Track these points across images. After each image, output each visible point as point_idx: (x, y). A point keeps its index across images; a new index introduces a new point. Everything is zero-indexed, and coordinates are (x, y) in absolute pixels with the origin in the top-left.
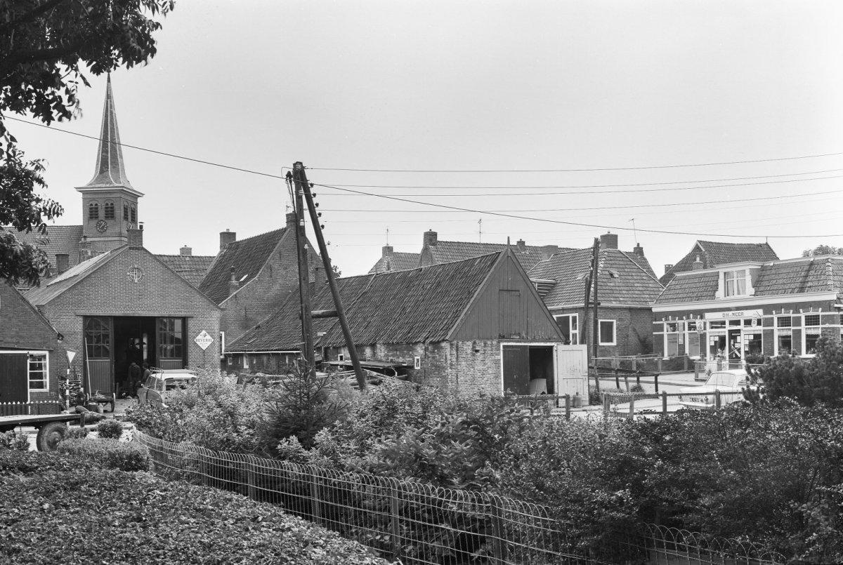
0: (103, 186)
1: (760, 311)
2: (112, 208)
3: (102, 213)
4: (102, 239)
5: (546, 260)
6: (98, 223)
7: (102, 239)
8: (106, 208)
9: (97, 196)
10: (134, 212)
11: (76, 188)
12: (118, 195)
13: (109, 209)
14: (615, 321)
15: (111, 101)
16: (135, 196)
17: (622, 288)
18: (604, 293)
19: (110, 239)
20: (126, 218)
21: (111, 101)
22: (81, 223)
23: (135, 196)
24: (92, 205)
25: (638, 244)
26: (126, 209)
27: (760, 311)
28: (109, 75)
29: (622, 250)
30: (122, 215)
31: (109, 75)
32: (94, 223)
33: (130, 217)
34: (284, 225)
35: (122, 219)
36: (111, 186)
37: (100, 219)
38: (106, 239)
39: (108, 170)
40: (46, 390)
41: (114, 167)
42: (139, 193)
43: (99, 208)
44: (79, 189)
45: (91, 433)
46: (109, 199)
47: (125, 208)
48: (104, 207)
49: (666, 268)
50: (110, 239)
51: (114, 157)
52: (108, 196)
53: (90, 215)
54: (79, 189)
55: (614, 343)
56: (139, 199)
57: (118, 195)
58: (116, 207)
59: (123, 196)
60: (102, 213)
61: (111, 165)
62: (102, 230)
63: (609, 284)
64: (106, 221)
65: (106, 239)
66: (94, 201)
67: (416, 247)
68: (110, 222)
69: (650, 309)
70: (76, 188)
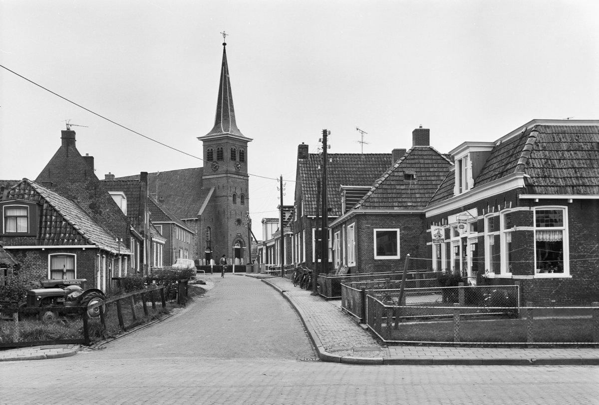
0: (216, 135)
1: (474, 212)
2: (222, 151)
3: (215, 156)
4: (215, 176)
5: (158, 183)
7: (215, 176)
8: (218, 152)
9: (212, 143)
10: (243, 154)
11: (198, 138)
12: (226, 141)
13: (220, 153)
14: (398, 230)
15: (225, 68)
16: (244, 142)
17: (416, 191)
18: (424, 193)
19: (220, 176)
20: (233, 158)
21: (225, 68)
22: (202, 166)
23: (244, 142)
24: (209, 150)
25: (68, 137)
27: (474, 212)
28: (224, 47)
30: (230, 156)
31: (224, 47)
33: (238, 159)
34: (391, 153)
37: (214, 160)
38: (218, 176)
41: (225, 120)
42: (249, 139)
46: (220, 144)
50: (220, 176)
51: (226, 111)
52: (220, 142)
53: (208, 158)
55: (377, 258)
56: (248, 143)
57: (226, 141)
58: (224, 151)
60: (215, 156)
61: (223, 118)
62: (215, 169)
63: (398, 187)
65: (218, 176)
67: (108, 174)
68: (220, 163)
69: (422, 215)
70: (198, 138)
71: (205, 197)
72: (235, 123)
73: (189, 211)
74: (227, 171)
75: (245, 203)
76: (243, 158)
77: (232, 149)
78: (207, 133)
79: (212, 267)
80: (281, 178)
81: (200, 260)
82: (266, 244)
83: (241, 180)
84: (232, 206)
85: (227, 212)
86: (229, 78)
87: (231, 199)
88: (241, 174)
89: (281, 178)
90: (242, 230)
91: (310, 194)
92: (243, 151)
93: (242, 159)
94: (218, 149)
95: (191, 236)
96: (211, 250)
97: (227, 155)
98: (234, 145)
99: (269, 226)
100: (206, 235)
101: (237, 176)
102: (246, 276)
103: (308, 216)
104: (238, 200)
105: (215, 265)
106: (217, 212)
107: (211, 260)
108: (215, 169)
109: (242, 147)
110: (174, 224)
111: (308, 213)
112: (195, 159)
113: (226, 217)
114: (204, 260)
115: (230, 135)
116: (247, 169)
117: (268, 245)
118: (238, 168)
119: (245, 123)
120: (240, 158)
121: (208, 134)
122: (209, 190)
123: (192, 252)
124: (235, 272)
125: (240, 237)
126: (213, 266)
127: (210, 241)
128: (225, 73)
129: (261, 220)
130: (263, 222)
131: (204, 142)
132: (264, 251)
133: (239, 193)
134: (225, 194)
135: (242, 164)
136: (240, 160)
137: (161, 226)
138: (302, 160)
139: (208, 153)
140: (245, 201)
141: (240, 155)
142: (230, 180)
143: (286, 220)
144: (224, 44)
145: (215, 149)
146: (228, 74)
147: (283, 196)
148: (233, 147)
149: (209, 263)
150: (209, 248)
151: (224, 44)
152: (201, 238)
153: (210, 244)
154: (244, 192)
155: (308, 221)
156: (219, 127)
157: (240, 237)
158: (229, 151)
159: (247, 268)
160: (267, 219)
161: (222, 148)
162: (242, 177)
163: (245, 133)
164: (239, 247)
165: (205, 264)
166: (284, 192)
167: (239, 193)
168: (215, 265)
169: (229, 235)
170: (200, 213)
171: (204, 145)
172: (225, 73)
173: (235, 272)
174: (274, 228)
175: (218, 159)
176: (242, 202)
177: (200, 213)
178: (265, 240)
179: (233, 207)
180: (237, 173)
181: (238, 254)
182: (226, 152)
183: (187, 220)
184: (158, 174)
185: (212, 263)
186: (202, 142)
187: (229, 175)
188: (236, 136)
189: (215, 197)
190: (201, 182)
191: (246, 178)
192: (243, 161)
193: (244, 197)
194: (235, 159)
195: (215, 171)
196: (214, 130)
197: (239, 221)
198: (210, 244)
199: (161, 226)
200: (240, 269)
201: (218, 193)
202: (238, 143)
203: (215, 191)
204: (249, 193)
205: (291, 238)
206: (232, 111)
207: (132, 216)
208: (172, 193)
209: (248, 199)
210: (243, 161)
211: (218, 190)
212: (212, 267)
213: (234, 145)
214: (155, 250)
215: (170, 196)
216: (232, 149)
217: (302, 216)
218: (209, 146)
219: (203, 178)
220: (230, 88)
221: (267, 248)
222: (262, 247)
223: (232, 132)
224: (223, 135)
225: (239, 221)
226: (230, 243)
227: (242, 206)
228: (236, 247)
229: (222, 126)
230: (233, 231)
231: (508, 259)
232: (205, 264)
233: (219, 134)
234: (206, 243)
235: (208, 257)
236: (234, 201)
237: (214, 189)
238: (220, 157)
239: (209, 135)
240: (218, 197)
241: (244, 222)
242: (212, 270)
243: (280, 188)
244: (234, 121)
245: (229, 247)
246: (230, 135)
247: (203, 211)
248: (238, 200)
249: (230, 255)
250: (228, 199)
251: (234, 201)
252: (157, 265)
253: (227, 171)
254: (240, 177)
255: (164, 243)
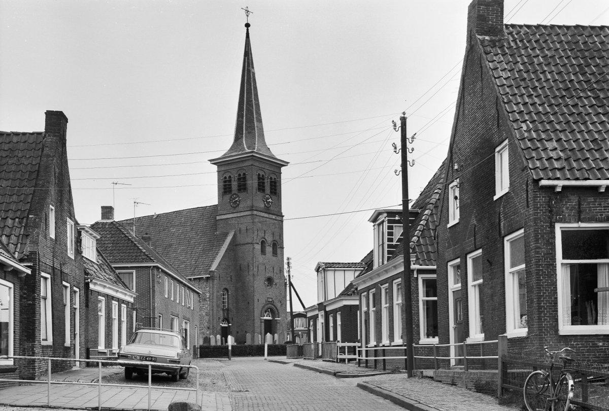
0: (236, 155)
3: (235, 185)
4: (235, 215)
6: (231, 197)
7: (235, 215)
12: (250, 163)
15: (248, 59)
16: (277, 166)
19: (242, 214)
20: (261, 188)
21: (248, 59)
22: (217, 203)
23: (277, 166)
26: (261, 179)
28: (248, 30)
29: (116, 221)
30: (256, 185)
31: (248, 30)
32: (227, 197)
35: (254, 190)
36: (244, 152)
38: (239, 215)
39: (242, 137)
40: (566, 327)
41: (249, 133)
42: (283, 161)
43: (233, 179)
44: (213, 161)
45: (202, 393)
46: (241, 168)
47: (259, 178)
48: (236, 178)
49: (506, 331)
50: (242, 214)
51: (250, 121)
52: (241, 165)
53: (224, 189)
54: (213, 161)
55: (558, 228)
56: (283, 169)
57: (250, 163)
58: (248, 177)
59: (257, 164)
60: (235, 185)
61: (246, 130)
62: (235, 206)
64: (239, 194)
65: (239, 215)
66: (227, 174)
68: (242, 195)
70: (210, 161)
71: (220, 246)
72: (264, 139)
73: (197, 267)
74: (252, 206)
75: (279, 255)
76: (276, 190)
77: (259, 175)
78: (223, 154)
79: (230, 348)
80: (404, 120)
81: (211, 336)
82: (325, 306)
83: (273, 221)
84: (260, 258)
85: (253, 266)
86: (254, 74)
87: (258, 247)
88: (272, 213)
89: (404, 120)
90: (272, 293)
91: (533, 122)
92: (275, 179)
93: (273, 191)
94: (240, 175)
95: (196, 295)
96: (229, 323)
97: (252, 183)
98: (262, 169)
99: (330, 275)
100: (222, 300)
101: (266, 215)
102: (296, 365)
103: (544, 182)
104: (269, 249)
105: (235, 344)
106: (238, 267)
107: (230, 337)
108: (235, 206)
109: (274, 173)
110: (158, 268)
111: (542, 175)
112: (206, 193)
113: (251, 273)
114: (219, 337)
115: (257, 153)
116: (281, 205)
117: (328, 309)
118: (268, 203)
119: (277, 139)
120: (271, 189)
121: (224, 155)
122: (226, 235)
123: (197, 322)
124: (269, 354)
125: (272, 303)
126: (233, 346)
127: (228, 310)
128: (248, 66)
129: (315, 266)
130: (318, 270)
131: (218, 167)
132: (321, 320)
133: (269, 239)
134: (250, 241)
135: (274, 197)
136: (271, 192)
137: (134, 272)
138: (487, 38)
139: (225, 182)
140: (279, 251)
141: (271, 185)
142: (256, 220)
143: (394, 243)
144: (247, 25)
145: (235, 176)
146: (253, 68)
147: (409, 168)
148: (262, 173)
149: (226, 341)
150: (226, 319)
151: (247, 25)
152: (215, 304)
153: (228, 314)
154: (277, 238)
155: (542, 199)
156: (241, 143)
157: (272, 303)
158: (255, 177)
159: (288, 350)
160: (326, 264)
161: (244, 174)
162: (274, 217)
163: (278, 152)
164: (270, 318)
165: (219, 344)
166: (410, 157)
167: (269, 239)
168: (235, 344)
169: (256, 301)
170: (213, 268)
171: (218, 172)
172: (248, 66)
173: (269, 354)
174: (339, 282)
175: (239, 190)
176: (275, 253)
177: (213, 268)
178: (322, 300)
179: (261, 261)
180: (267, 210)
181: (270, 327)
182: (251, 179)
183: (195, 279)
184: (155, 217)
185: (231, 341)
186: (215, 167)
187: (255, 212)
188: (266, 156)
189: (234, 245)
190: (215, 224)
191: (279, 218)
192: (275, 193)
193: (278, 246)
194: (264, 191)
195: (235, 208)
196: (233, 148)
197: (270, 281)
198: (228, 314)
199: (134, 272)
200: (277, 350)
201: (241, 239)
202: (267, 167)
203: (234, 237)
204: (282, 182)
205: (417, 278)
206: (260, 121)
207: (10, 214)
208: (174, 241)
209: (283, 248)
210: (275, 193)
211: (238, 235)
212: (230, 348)
213: (262, 169)
214: (102, 314)
215: (170, 245)
216: (259, 175)
217: (499, 194)
218: (226, 171)
219: (218, 218)
220: (255, 88)
221: (327, 314)
222: (316, 312)
223: (259, 150)
224: (247, 153)
225: (270, 281)
226: (257, 312)
227: (274, 258)
228: (265, 318)
229: (244, 142)
230: (261, 294)
231: (9, 336)
232: (219, 344)
233: (240, 153)
234: (221, 312)
235: (225, 333)
236: (263, 251)
237: (233, 233)
238: (243, 187)
239: (227, 156)
240: (240, 245)
241: (278, 281)
242: (230, 353)
243: (399, 146)
244: (262, 135)
245: (255, 318)
246: (257, 153)
247: (216, 266)
248: (269, 249)
249: (257, 330)
250: (254, 248)
251: (263, 251)
252: (109, 344)
253: (252, 206)
254: (271, 216)
255: (132, 300)
